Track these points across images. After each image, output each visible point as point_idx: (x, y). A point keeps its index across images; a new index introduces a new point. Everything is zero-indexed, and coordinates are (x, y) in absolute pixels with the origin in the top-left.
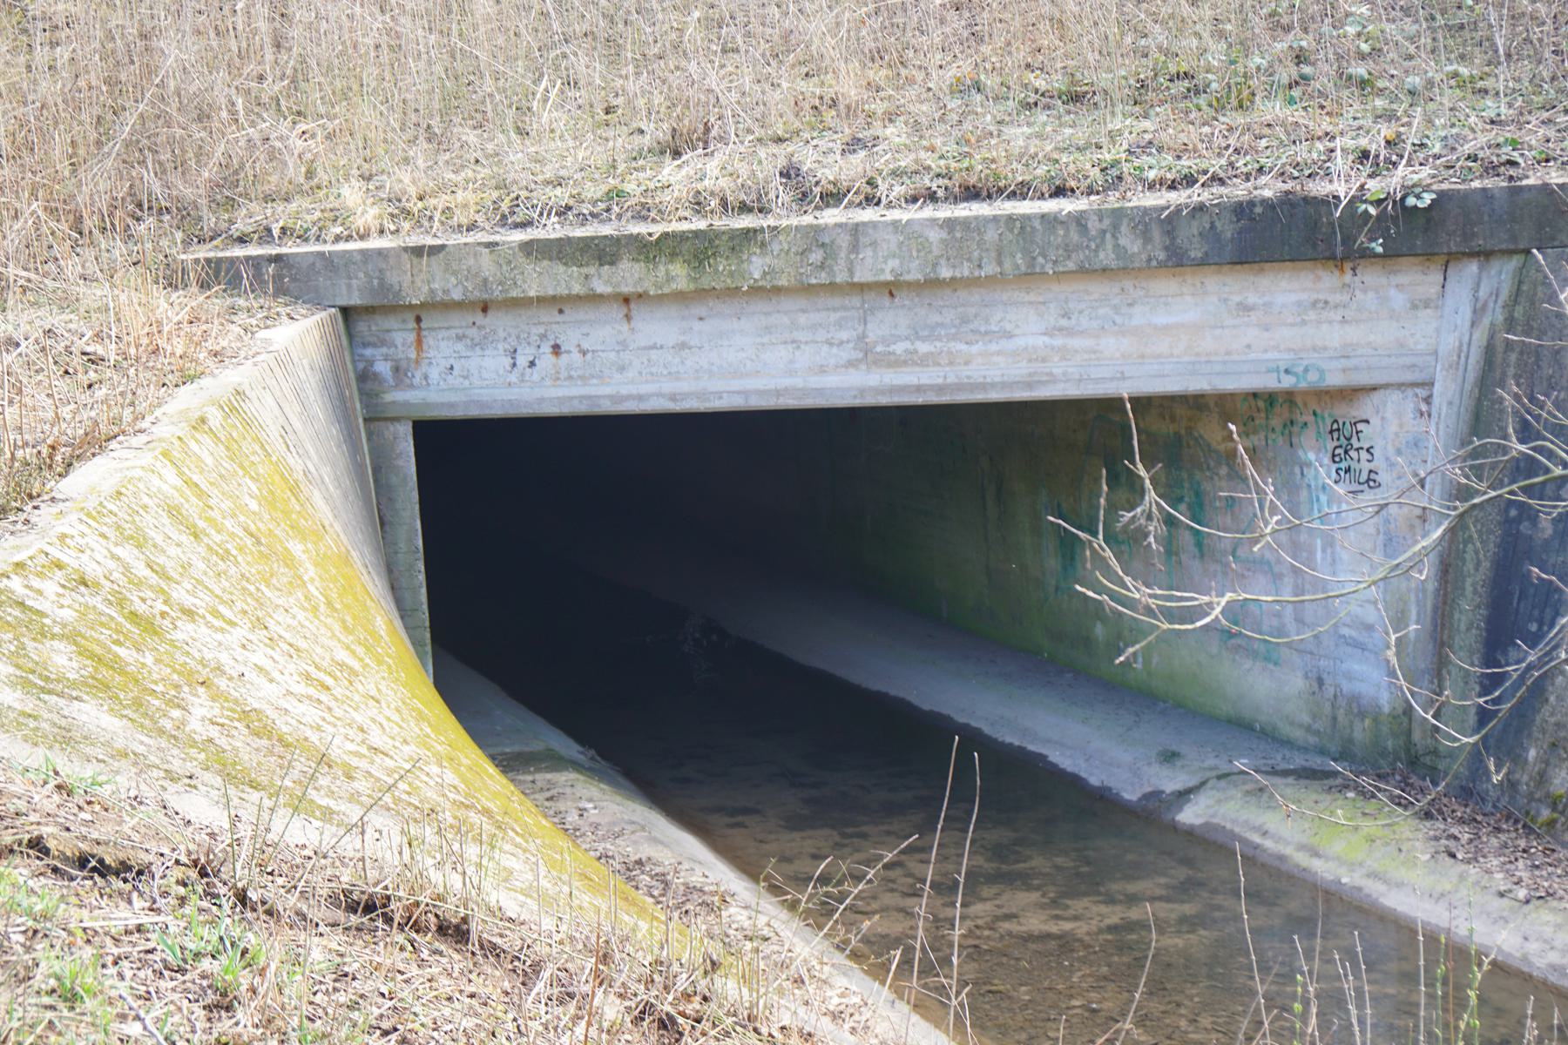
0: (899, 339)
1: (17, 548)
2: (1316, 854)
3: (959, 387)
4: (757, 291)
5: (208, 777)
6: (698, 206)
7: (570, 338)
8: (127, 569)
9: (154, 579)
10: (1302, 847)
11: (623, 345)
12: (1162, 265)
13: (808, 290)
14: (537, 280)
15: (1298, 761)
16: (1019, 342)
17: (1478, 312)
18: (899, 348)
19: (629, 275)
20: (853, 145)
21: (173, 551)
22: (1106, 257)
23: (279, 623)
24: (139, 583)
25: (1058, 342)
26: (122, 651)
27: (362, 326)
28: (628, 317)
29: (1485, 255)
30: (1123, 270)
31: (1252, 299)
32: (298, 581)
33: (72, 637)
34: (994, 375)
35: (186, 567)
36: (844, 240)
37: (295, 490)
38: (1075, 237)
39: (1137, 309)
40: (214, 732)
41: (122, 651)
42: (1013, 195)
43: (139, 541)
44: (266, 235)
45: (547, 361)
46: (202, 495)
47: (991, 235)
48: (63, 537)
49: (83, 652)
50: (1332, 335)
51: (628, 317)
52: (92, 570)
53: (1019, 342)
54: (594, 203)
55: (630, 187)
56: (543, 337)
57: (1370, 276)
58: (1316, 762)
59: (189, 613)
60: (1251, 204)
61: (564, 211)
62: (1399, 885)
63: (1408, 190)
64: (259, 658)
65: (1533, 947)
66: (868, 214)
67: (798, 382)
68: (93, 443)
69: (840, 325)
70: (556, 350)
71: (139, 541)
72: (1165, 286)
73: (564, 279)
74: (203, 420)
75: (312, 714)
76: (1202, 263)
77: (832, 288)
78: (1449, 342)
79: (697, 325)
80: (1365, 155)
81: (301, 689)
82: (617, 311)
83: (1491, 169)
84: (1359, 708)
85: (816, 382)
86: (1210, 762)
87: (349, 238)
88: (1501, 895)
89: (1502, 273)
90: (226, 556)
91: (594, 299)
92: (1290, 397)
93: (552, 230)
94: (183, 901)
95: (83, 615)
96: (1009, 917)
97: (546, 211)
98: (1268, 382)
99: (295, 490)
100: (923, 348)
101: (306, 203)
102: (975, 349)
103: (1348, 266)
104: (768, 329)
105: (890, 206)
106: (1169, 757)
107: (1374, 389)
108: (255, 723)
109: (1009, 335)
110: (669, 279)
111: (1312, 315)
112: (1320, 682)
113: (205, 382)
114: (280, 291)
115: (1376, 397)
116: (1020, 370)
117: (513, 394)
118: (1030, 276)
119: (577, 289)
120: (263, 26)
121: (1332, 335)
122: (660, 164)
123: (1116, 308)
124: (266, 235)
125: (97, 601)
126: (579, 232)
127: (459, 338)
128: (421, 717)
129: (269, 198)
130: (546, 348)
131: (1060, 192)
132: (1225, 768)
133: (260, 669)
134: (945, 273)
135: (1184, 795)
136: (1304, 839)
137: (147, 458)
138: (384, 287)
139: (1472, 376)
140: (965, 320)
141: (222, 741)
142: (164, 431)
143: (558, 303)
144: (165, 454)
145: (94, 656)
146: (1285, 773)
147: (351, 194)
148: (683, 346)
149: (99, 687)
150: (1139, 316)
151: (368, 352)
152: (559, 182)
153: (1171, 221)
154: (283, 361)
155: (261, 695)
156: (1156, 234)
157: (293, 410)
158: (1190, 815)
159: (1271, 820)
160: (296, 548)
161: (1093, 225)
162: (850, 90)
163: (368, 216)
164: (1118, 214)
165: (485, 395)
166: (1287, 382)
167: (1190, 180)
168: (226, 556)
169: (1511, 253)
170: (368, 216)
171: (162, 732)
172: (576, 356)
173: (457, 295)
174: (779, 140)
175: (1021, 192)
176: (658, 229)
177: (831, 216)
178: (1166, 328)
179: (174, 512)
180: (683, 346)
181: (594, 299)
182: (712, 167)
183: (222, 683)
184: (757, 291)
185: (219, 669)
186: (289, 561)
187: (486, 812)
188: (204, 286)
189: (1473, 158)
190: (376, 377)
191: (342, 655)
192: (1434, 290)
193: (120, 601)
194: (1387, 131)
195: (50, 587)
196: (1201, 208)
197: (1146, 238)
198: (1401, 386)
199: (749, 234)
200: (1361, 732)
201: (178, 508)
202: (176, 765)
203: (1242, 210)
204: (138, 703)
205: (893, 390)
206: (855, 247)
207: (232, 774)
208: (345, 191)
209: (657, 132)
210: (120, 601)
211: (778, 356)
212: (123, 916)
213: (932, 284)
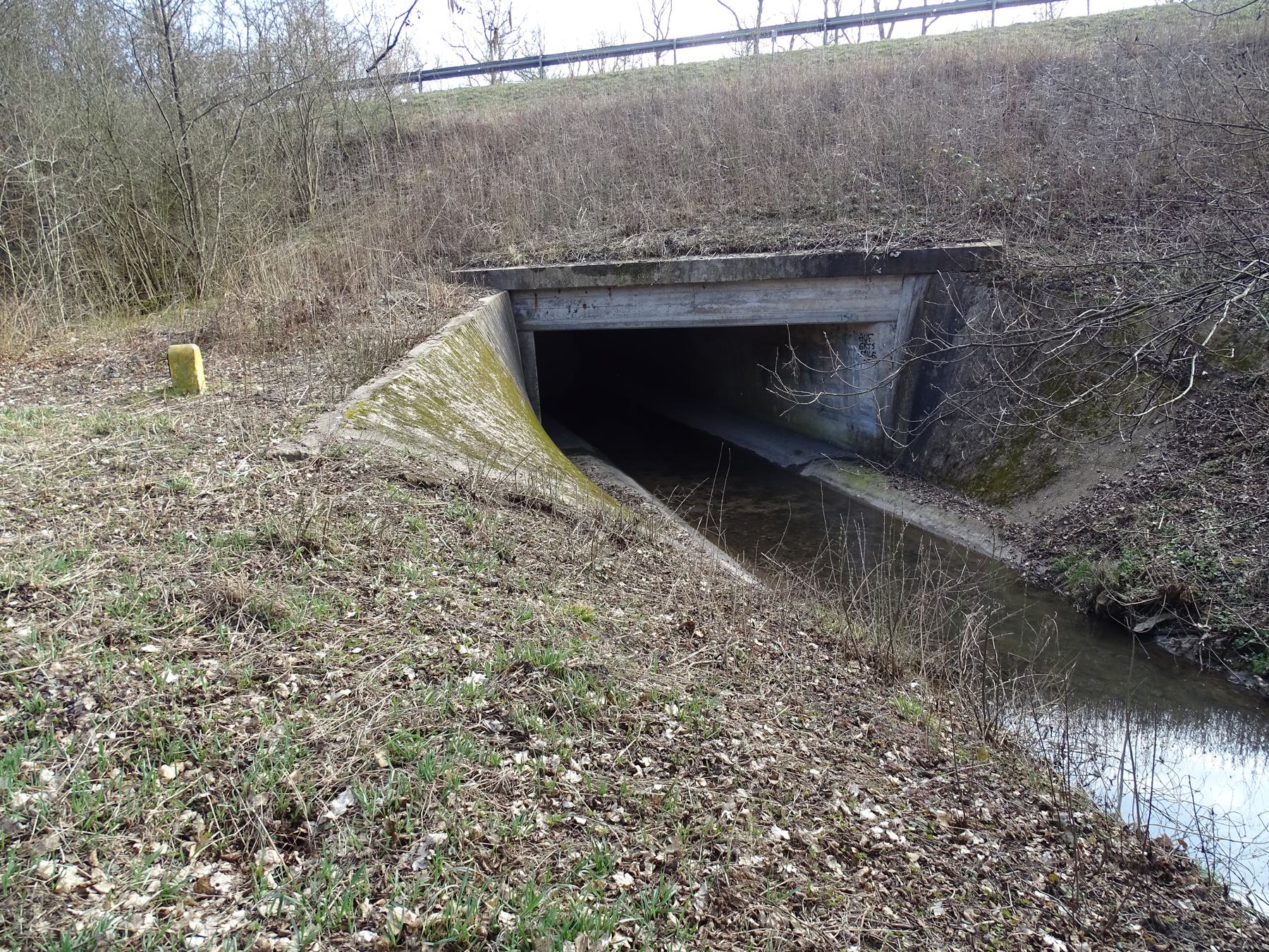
0: (706, 303)
1: (395, 374)
3: (727, 321)
6: (635, 254)
7: (589, 302)
8: (433, 382)
9: (443, 386)
10: (844, 484)
13: (674, 285)
14: (577, 281)
15: (843, 454)
16: (749, 305)
17: (914, 295)
18: (707, 306)
19: (610, 279)
20: (691, 233)
21: (449, 376)
22: (781, 274)
24: (438, 387)
25: (763, 305)
26: (432, 411)
27: (516, 297)
28: (610, 295)
29: (917, 275)
30: (787, 279)
31: (833, 290)
32: (493, 388)
33: (414, 405)
34: (740, 316)
35: (454, 382)
36: (687, 267)
37: (492, 355)
40: (464, 439)
41: (432, 411)
43: (438, 372)
45: (581, 310)
46: (459, 356)
48: (411, 370)
49: (418, 411)
50: (862, 303)
51: (610, 295)
52: (421, 382)
53: (749, 305)
56: (580, 301)
57: (876, 282)
59: (455, 398)
60: (834, 255)
63: (891, 250)
64: (479, 414)
65: (923, 519)
66: (696, 258)
67: (670, 318)
68: (421, 338)
69: (685, 298)
70: (585, 306)
71: (438, 372)
72: (802, 285)
73: (588, 281)
74: (460, 330)
75: (499, 433)
76: (816, 277)
77: (683, 285)
78: (904, 306)
79: (635, 298)
80: (876, 237)
81: (494, 425)
82: (606, 293)
83: (921, 243)
84: (865, 436)
85: (676, 318)
86: (813, 454)
87: (511, 265)
89: (924, 282)
90: (468, 378)
91: (598, 288)
93: (583, 263)
94: (453, 497)
95: (418, 398)
96: (740, 507)
98: (838, 320)
100: (715, 306)
104: (660, 300)
105: (704, 255)
106: (798, 453)
107: (876, 323)
108: (479, 437)
110: (625, 281)
111: (855, 296)
112: (852, 427)
113: (461, 316)
114: (487, 284)
115: (876, 326)
116: (749, 315)
117: (569, 322)
118: (754, 281)
119: (592, 284)
120: (480, 187)
121: (862, 303)
122: (622, 239)
124: (481, 264)
125: (423, 393)
128: (536, 436)
129: (482, 251)
130: (581, 306)
131: (765, 250)
132: (818, 456)
133: (480, 418)
134: (723, 279)
135: (803, 466)
137: (440, 343)
139: (911, 318)
140: (730, 296)
142: (446, 334)
143: (585, 289)
144: (447, 342)
145: (421, 412)
146: (839, 459)
147: (512, 249)
148: (629, 305)
149: (423, 423)
150: (793, 295)
152: (585, 245)
153: (805, 261)
154: (488, 309)
155: (481, 426)
158: (805, 473)
159: (833, 475)
160: (493, 376)
161: (777, 262)
162: (690, 212)
163: (518, 257)
164: (786, 258)
165: (559, 322)
166: (845, 320)
167: (812, 246)
168: (468, 378)
171: (446, 439)
172: (592, 308)
173: (549, 286)
175: (751, 250)
176: (621, 263)
177: (683, 258)
179: (450, 362)
180: (629, 305)
181: (598, 288)
182: (641, 240)
183: (467, 423)
185: (466, 417)
186: (490, 380)
187: (559, 468)
188: (460, 282)
189: (914, 239)
190: (521, 315)
191: (509, 413)
193: (431, 393)
195: (406, 388)
197: (796, 267)
198: (885, 322)
200: (866, 444)
201: (451, 361)
202: (451, 450)
203: (831, 257)
204: (437, 429)
205: (704, 321)
206: (691, 270)
207: (470, 454)
208: (510, 248)
209: (620, 227)
210: (431, 393)
211: (663, 309)
212: (436, 501)
213: (718, 284)
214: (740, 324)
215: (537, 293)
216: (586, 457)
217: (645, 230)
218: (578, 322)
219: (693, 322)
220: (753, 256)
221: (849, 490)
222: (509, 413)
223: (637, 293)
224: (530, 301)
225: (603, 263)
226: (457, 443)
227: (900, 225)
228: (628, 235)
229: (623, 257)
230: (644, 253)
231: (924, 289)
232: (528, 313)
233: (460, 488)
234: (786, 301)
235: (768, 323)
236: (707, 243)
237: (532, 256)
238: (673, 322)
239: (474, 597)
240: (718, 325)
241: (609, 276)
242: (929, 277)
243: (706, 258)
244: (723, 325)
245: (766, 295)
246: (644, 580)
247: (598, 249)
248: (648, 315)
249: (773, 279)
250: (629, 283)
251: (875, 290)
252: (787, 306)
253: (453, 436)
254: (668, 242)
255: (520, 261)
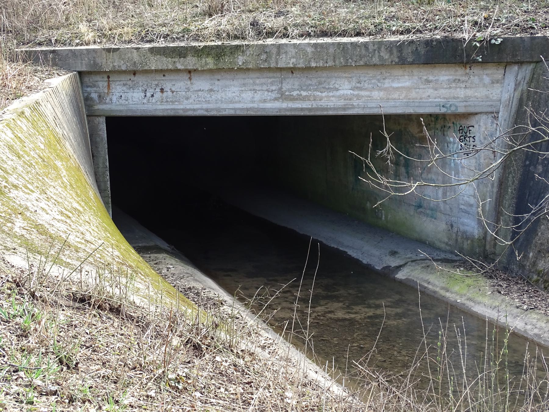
0: (294, 90)
2: (448, 291)
3: (317, 109)
4: (240, 70)
5: (21, 249)
6: (218, 35)
7: (168, 86)
10: (442, 288)
11: (188, 89)
12: (397, 64)
14: (154, 63)
15: (443, 256)
16: (341, 92)
17: (517, 85)
18: (295, 93)
19: (191, 62)
20: (279, 14)
21: (10, 163)
22: (375, 60)
23: (51, 192)
25: (356, 93)
27: (86, 79)
29: (521, 63)
31: (431, 78)
32: (59, 176)
34: (331, 104)
35: (15, 169)
36: (274, 51)
37: (59, 141)
38: (364, 52)
39: (387, 81)
40: (24, 232)
42: (340, 35)
44: (49, 42)
45: (158, 95)
46: (21, 141)
47: (331, 50)
50: (461, 93)
53: (341, 92)
54: (178, 33)
55: (192, 28)
56: (157, 85)
57: (476, 70)
58: (449, 256)
59: (16, 187)
60: (432, 41)
61: (166, 37)
62: (479, 303)
63: (492, 37)
64: (43, 204)
65: (529, 327)
66: (284, 41)
67: (255, 105)
69: (272, 84)
70: (162, 90)
72: (397, 72)
73: (166, 63)
74: (23, 113)
75: (63, 227)
76: (412, 63)
77: (269, 69)
79: (217, 83)
80: (476, 23)
81: (59, 217)
82: (186, 76)
83: (524, 30)
84: (466, 236)
85: (262, 105)
88: (518, 307)
89: (526, 71)
90: (31, 165)
91: (177, 71)
92: (444, 116)
93: (161, 44)
94: (9, 295)
96: (330, 312)
97: (159, 36)
99: (59, 141)
100: (304, 93)
101: (65, 31)
102: (324, 94)
103: (468, 66)
104: (244, 85)
105: (292, 38)
106: (394, 253)
107: (476, 114)
108: (41, 230)
109: (337, 90)
110: (206, 64)
111: (454, 85)
112: (452, 226)
113: (24, 98)
114: (55, 64)
115: (477, 117)
116: (341, 103)
118: (346, 67)
119: (170, 67)
121: (461, 93)
122: (204, 19)
123: (379, 80)
124: (49, 42)
126: (172, 45)
127: (124, 85)
128: (106, 230)
129: (50, 28)
130: (158, 90)
131: (358, 34)
132: (414, 258)
133: (43, 209)
134: (313, 65)
136: (443, 285)
138: (95, 64)
139: (514, 109)
140: (320, 83)
141: (27, 236)
143: (163, 72)
144: (8, 125)
147: (83, 28)
148: (211, 90)
150: (387, 84)
151: (89, 89)
152: (164, 25)
153: (400, 47)
154: (55, 91)
155: (43, 219)
156: (395, 51)
157: (59, 111)
158: (401, 275)
159: (432, 278)
160: (59, 164)
161: (371, 48)
164: (381, 43)
165: (134, 107)
166: (443, 110)
167: (408, 31)
168: (31, 165)
169: (530, 62)
170: (90, 36)
172: (170, 93)
173: (124, 68)
174: (250, 11)
175: (344, 34)
176: (202, 44)
177: (270, 41)
178: (397, 89)
180: (211, 90)
181: (177, 71)
182: (224, 21)
183: (28, 214)
184: (240, 70)
185: (27, 208)
186: (56, 168)
189: (516, 25)
190: (92, 99)
191: (75, 205)
192: (500, 76)
194: (485, 14)
196: (412, 42)
197: (391, 52)
198: (486, 113)
199: (237, 47)
200: (466, 245)
202: (9, 245)
203: (428, 43)
205: (292, 109)
206: (278, 54)
207: (31, 248)
208: (81, 26)
211: (248, 95)
214: (331, 113)
215: (109, 75)
216: (161, 256)
217: (229, 10)
218: (155, 107)
219: (280, 110)
220: (345, 40)
221: (448, 294)
222: (75, 205)
223: (219, 77)
224: (102, 84)
225: (182, 44)
226: (16, 236)
227: (501, 11)
228: (210, 15)
229: (205, 39)
230: (228, 35)
231: (527, 78)
232: (100, 96)
233: (18, 285)
234: (380, 89)
235: (361, 112)
236: (296, 25)
237: (105, 36)
238: (258, 109)
239: (30, 406)
240: (307, 113)
241: (189, 58)
242: (532, 66)
243: (295, 41)
244: (312, 113)
245: (359, 82)
246: (222, 390)
247: (177, 29)
248: (232, 102)
249: (367, 66)
250: (211, 66)
251: (476, 79)
252: (382, 94)
253: (11, 229)
254: (254, 24)
255: (92, 40)
